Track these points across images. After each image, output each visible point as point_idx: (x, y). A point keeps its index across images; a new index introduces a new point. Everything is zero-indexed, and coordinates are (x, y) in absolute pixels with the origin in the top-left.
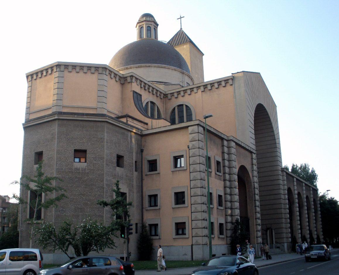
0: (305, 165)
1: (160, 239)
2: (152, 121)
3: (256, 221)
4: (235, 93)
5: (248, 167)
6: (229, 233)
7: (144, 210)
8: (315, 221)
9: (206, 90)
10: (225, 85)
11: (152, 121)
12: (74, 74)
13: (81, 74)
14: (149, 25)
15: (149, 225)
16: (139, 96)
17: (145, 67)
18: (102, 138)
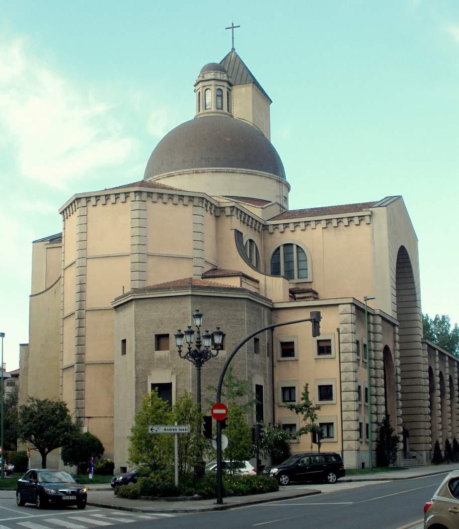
0: (443, 317)
1: (298, 443)
2: (265, 278)
3: (398, 419)
4: (373, 236)
5: (391, 347)
6: (375, 436)
7: (276, 406)
8: (450, 415)
9: (329, 225)
10: (360, 223)
11: (265, 278)
12: (159, 205)
13: (170, 205)
14: (221, 88)
15: (283, 425)
16: (240, 234)
17: (227, 172)
18: (242, 319)
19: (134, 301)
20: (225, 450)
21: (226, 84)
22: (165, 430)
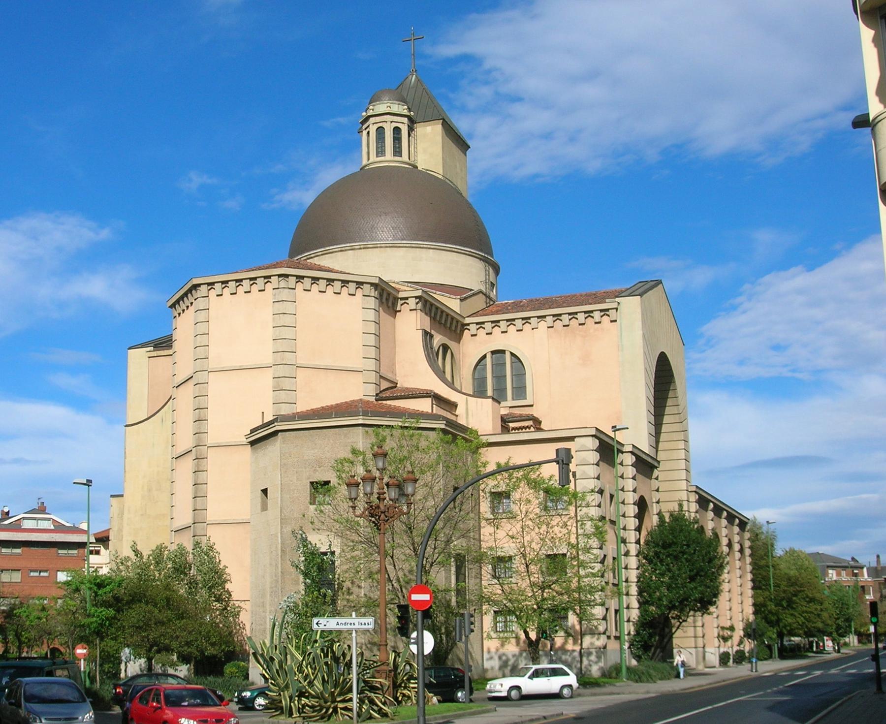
19: (280, 434)
20: (748, 652)
21: (405, 120)
22: (338, 624)
